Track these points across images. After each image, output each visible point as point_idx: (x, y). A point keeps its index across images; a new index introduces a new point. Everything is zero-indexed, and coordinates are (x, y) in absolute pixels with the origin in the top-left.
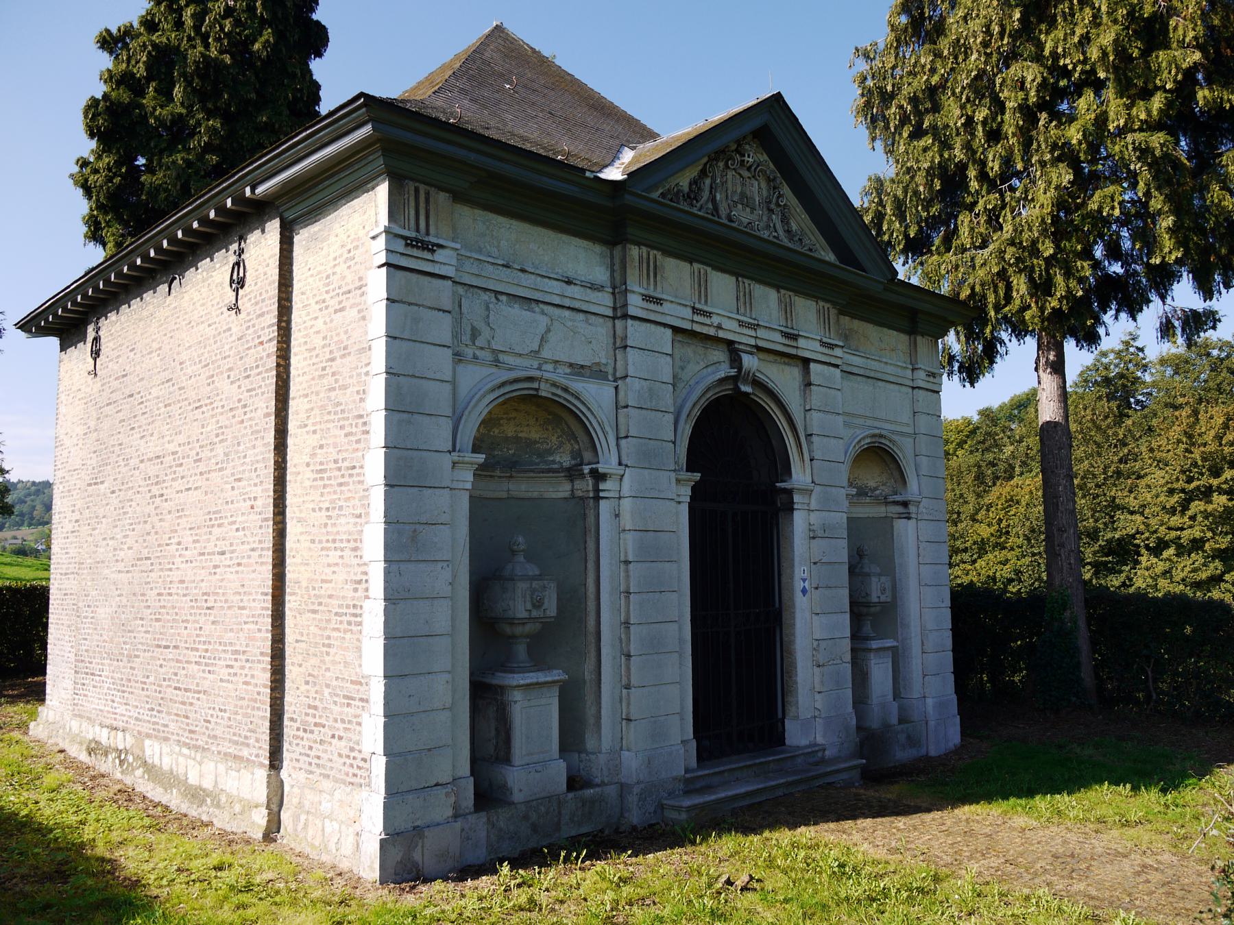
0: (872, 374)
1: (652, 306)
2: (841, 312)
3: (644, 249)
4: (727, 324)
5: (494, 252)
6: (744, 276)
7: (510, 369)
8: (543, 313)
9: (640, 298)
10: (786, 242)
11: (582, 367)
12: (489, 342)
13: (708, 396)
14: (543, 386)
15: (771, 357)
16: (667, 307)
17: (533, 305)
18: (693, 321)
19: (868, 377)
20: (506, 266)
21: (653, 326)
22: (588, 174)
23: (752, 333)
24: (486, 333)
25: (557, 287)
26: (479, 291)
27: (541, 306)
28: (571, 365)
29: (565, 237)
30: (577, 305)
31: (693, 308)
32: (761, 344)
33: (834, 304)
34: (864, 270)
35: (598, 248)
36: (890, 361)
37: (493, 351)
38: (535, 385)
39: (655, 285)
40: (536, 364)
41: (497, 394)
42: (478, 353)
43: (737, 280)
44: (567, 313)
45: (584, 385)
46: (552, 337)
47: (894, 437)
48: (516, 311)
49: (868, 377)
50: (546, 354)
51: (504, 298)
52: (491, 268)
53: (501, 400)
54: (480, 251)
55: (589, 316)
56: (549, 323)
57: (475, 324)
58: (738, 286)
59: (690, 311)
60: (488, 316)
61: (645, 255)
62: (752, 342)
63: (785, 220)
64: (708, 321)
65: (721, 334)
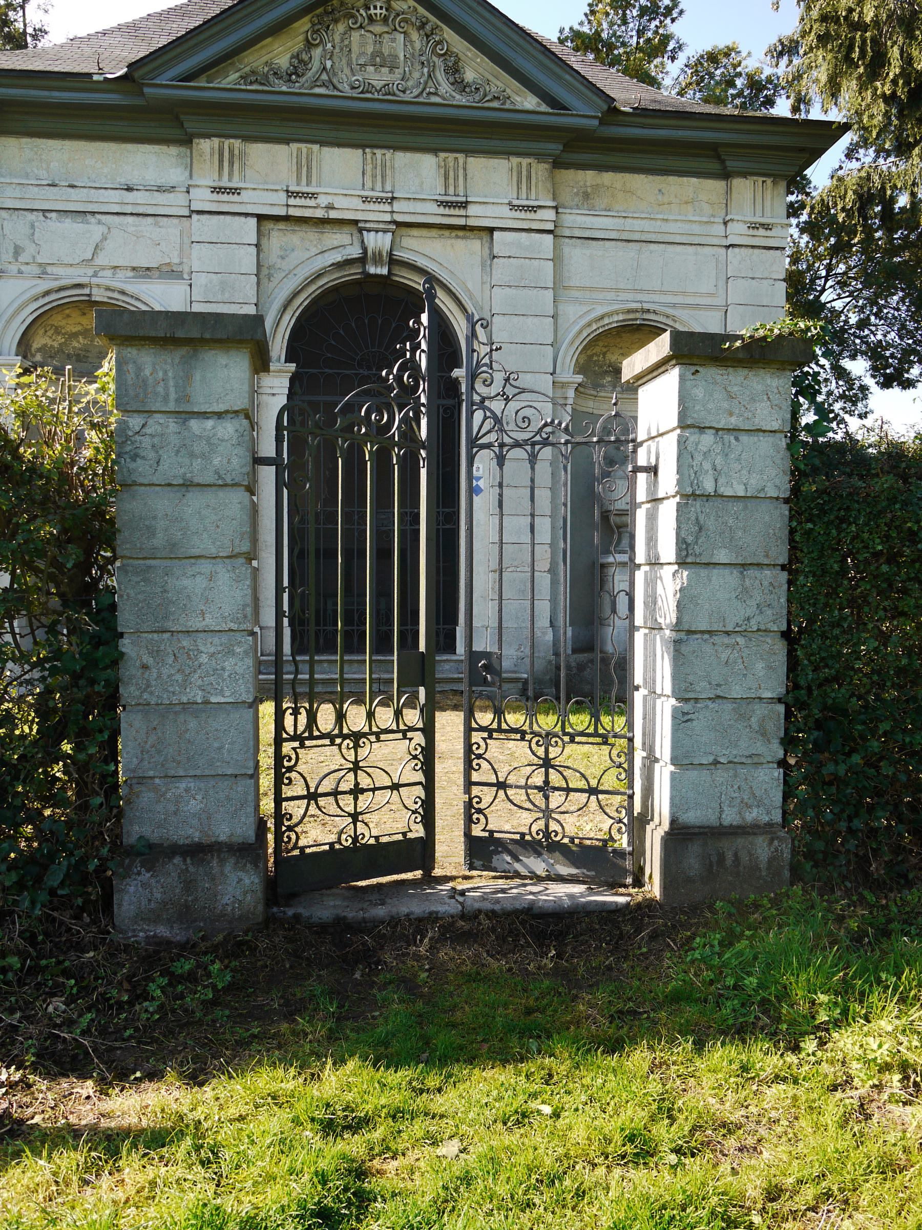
0: (636, 237)
1: (225, 197)
2: (558, 164)
3: (216, 141)
4: (339, 202)
5: (43, 174)
6: (372, 147)
7: (56, 279)
8: (99, 222)
9: (508, 207)
10: (460, 99)
11: (148, 269)
12: (34, 257)
13: (321, 282)
14: (95, 291)
15: (434, 232)
16: (245, 196)
17: (89, 216)
18: (288, 206)
19: (629, 241)
20: (53, 185)
21: (228, 218)
22: (95, 78)
23: (387, 208)
24: (31, 249)
25: (115, 196)
26: (25, 213)
27: (98, 216)
28: (134, 269)
29: (130, 147)
30: (141, 210)
31: (287, 191)
32: (399, 218)
33: (540, 156)
34: (566, 108)
35: (173, 150)
36: (671, 217)
37: (40, 265)
38: (87, 291)
39: (529, 188)
40: (90, 272)
41: (42, 302)
42: (23, 268)
43: (364, 153)
44: (130, 219)
45: (148, 286)
46: (109, 245)
47: (670, 311)
48: (69, 226)
49: (629, 241)
50: (101, 260)
51: (54, 215)
52: (36, 189)
53: (580, 348)
54: (27, 176)
55: (159, 218)
56: (106, 231)
57: (18, 243)
58: (364, 160)
59: (284, 195)
60: (33, 234)
61: (216, 146)
62: (388, 217)
63: (454, 70)
64: (312, 203)
65: (333, 215)
